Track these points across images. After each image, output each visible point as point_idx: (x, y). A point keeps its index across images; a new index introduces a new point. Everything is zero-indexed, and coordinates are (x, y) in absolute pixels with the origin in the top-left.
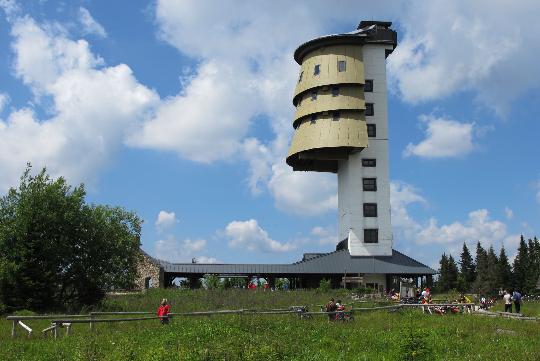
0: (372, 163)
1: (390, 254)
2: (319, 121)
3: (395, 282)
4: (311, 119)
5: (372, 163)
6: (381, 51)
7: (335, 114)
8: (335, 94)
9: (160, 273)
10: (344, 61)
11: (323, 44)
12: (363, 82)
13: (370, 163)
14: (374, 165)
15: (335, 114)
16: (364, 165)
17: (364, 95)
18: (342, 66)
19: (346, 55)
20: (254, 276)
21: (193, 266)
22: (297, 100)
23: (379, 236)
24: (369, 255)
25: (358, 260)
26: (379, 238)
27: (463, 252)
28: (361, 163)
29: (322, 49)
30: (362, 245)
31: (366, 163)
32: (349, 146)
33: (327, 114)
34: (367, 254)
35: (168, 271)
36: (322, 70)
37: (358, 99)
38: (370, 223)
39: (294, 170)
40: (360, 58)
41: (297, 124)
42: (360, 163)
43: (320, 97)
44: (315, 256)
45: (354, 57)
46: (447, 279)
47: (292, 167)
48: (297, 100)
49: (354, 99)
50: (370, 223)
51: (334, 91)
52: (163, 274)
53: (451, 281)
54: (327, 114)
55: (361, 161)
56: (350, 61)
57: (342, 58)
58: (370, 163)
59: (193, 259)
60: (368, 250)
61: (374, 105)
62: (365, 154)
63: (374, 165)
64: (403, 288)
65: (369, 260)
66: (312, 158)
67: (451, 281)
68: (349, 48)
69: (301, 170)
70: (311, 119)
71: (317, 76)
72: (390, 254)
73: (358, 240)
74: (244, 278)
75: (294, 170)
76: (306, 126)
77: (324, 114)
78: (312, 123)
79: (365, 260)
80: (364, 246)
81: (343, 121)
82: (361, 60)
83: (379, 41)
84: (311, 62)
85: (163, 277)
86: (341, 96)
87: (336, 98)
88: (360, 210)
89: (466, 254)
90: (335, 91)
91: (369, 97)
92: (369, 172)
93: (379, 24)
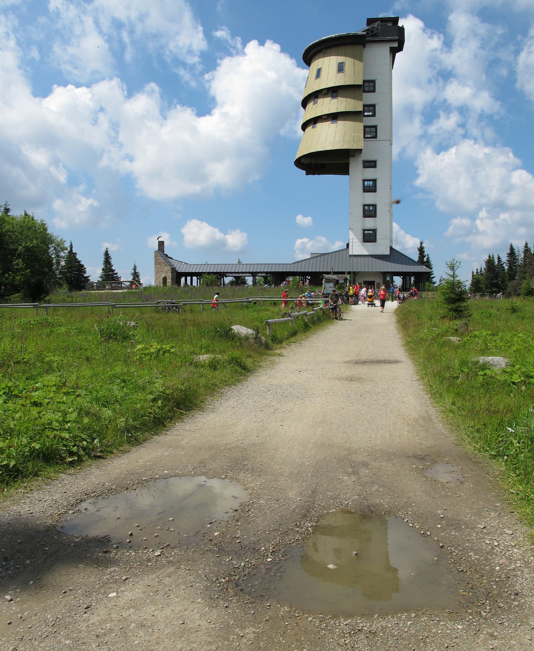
0: (372, 164)
1: (388, 252)
2: (319, 125)
3: (388, 279)
4: (313, 123)
5: (372, 164)
6: (384, 50)
7: (334, 117)
8: (333, 97)
9: (172, 273)
10: (343, 63)
11: (324, 47)
12: (361, 83)
13: (371, 164)
14: (375, 166)
15: (334, 117)
16: (365, 167)
17: (362, 96)
18: (341, 68)
19: (345, 56)
20: (259, 275)
21: (238, 266)
22: (305, 103)
23: (377, 236)
24: (367, 254)
25: (359, 259)
26: (377, 238)
27: (509, 252)
28: (361, 165)
29: (324, 51)
30: (361, 245)
31: (367, 164)
32: (343, 148)
33: (326, 117)
34: (366, 253)
35: (179, 271)
36: (323, 73)
37: (356, 101)
38: (370, 223)
39: (307, 174)
40: (359, 57)
41: (304, 127)
42: (361, 165)
43: (320, 101)
44: (316, 255)
45: (354, 56)
46: (487, 278)
47: (305, 171)
48: (305, 103)
49: (352, 101)
50: (370, 223)
51: (333, 94)
52: (175, 274)
53: (491, 280)
54: (326, 117)
55: (362, 163)
56: (348, 61)
57: (341, 59)
58: (371, 164)
59: (239, 260)
60: (367, 250)
61: (376, 106)
62: (366, 156)
63: (375, 166)
64: (327, 284)
65: (366, 259)
66: (314, 162)
67: (491, 280)
68: (349, 49)
69: (314, 174)
70: (313, 123)
71: (318, 80)
72: (388, 252)
73: (357, 240)
74: (263, 276)
75: (307, 174)
76: (309, 129)
77: (323, 117)
78: (313, 128)
79: (363, 259)
80: (363, 245)
81: (341, 124)
82: (361, 60)
83: (381, 38)
84: (317, 63)
85: (175, 277)
86: (339, 98)
87: (335, 101)
88: (360, 212)
89: (512, 253)
90: (334, 94)
91: (369, 98)
92: (370, 173)
93: (384, 20)
